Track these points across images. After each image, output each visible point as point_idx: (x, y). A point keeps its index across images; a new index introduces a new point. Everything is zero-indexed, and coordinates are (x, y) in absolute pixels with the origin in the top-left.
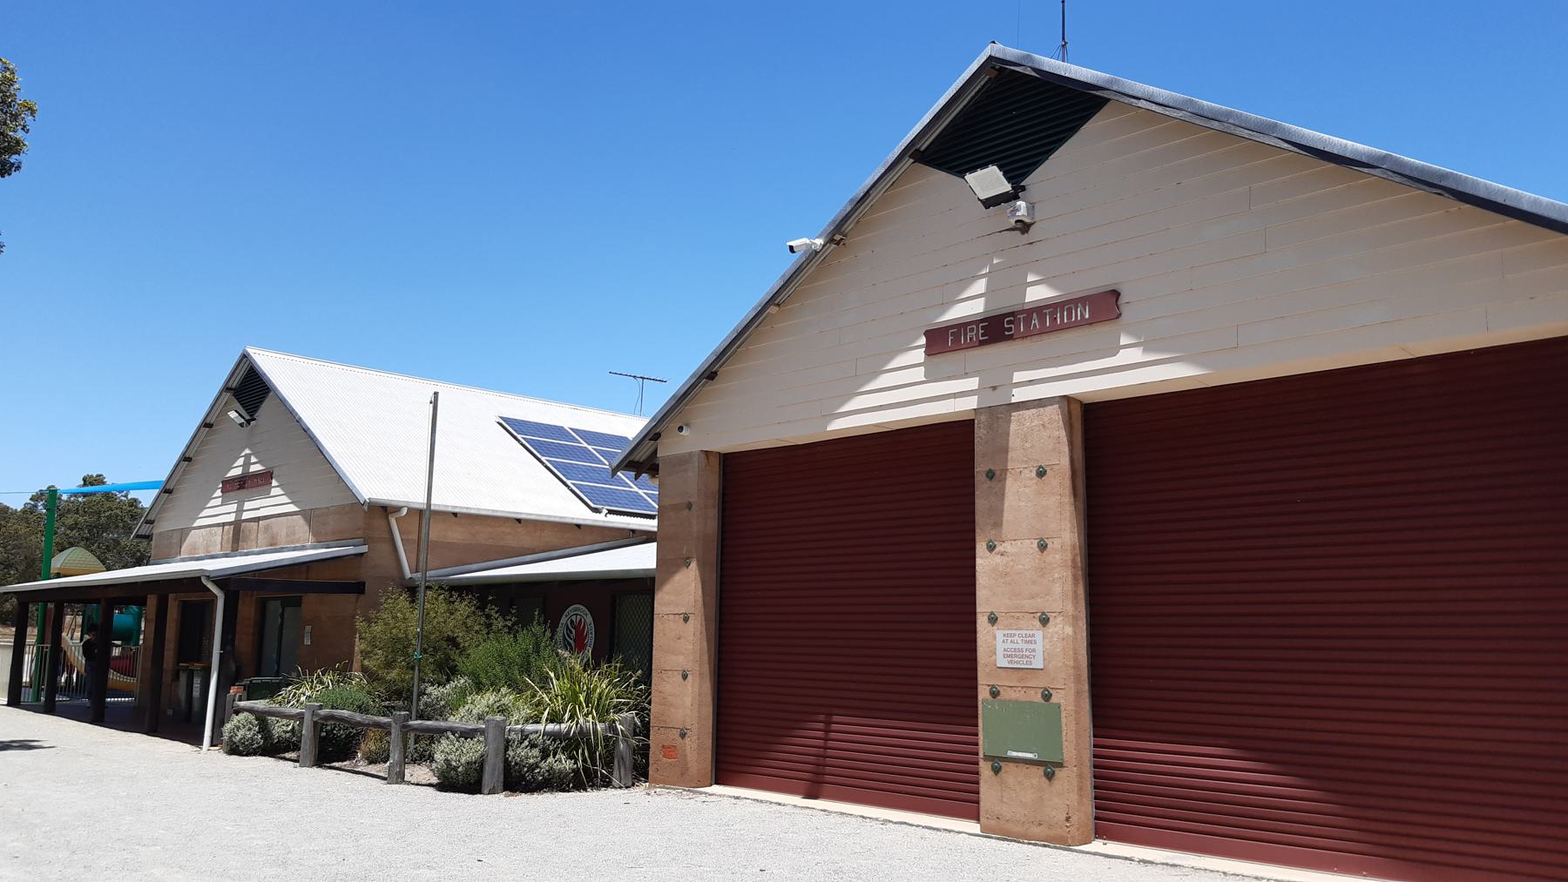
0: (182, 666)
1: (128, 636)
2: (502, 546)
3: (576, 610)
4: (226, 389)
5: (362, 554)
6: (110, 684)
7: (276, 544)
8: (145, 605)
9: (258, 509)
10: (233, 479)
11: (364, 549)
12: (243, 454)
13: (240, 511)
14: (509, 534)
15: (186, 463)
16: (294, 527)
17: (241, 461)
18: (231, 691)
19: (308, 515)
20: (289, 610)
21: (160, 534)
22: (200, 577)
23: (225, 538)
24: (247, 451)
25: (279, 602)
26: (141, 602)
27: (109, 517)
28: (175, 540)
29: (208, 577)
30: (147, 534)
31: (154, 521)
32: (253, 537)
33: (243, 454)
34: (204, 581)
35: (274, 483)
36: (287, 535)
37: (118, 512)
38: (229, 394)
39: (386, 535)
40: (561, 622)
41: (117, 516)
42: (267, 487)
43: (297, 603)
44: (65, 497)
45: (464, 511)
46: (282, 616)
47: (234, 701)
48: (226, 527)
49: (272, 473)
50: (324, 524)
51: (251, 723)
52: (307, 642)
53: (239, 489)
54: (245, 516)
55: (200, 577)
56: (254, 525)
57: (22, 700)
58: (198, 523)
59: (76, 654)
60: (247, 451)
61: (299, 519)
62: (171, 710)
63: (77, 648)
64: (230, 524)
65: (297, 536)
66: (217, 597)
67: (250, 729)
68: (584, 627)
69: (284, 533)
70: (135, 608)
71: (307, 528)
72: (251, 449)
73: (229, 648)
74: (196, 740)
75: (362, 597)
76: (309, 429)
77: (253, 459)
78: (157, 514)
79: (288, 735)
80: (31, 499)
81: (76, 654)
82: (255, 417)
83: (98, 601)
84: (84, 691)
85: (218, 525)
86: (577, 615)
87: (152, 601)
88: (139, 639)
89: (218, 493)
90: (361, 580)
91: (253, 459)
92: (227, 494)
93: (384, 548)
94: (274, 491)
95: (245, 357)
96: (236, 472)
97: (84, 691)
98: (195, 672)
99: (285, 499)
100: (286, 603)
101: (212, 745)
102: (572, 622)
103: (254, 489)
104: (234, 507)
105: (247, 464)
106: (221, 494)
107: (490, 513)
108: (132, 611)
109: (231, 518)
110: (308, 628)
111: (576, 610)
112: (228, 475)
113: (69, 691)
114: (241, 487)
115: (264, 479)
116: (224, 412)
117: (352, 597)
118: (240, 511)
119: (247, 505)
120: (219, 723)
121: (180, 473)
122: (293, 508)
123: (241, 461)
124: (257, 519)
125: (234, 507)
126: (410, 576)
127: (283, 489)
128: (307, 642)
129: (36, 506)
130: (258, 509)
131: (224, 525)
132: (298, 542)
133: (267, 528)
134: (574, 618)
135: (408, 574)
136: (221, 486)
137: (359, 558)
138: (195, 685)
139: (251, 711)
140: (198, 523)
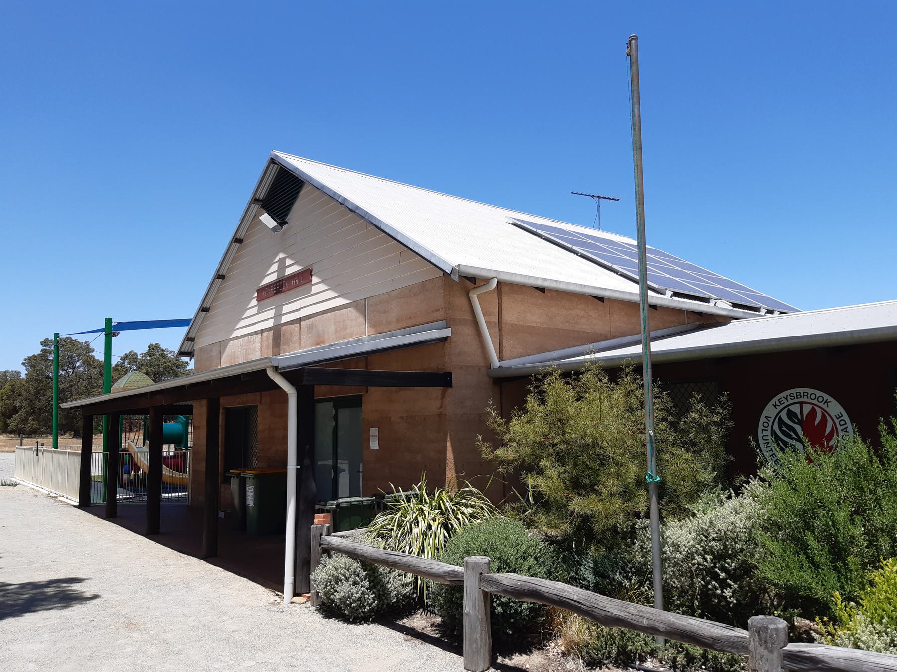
0: (233, 473)
1: (179, 440)
2: (578, 332)
3: (798, 395)
4: (255, 200)
5: (445, 339)
6: (164, 479)
7: (324, 343)
8: (191, 413)
9: (299, 310)
10: (268, 286)
11: (447, 332)
12: (277, 260)
13: (278, 315)
14: (582, 317)
15: (221, 280)
16: (344, 321)
17: (275, 267)
18: (316, 521)
19: (361, 306)
20: (345, 415)
21: (201, 349)
22: (264, 371)
23: (264, 344)
24: (281, 256)
25: (331, 404)
26: (188, 411)
27: (164, 368)
28: (215, 353)
29: (276, 369)
30: (189, 351)
31: (194, 338)
32: (295, 338)
33: (277, 260)
34: (271, 374)
35: (315, 279)
36: (336, 331)
37: (169, 364)
38: (257, 206)
39: (468, 316)
40: (765, 413)
41: (169, 366)
42: (308, 285)
43: (356, 402)
44: (139, 357)
45: (553, 285)
46: (336, 417)
47: (321, 535)
48: (265, 334)
49: (312, 271)
50: (385, 312)
51: (355, 574)
52: (374, 445)
53: (275, 294)
54: (285, 319)
55: (264, 371)
56: (296, 327)
57: (92, 502)
58: (236, 334)
59: (142, 459)
60: (281, 256)
61: (351, 312)
62: (220, 516)
63: (142, 454)
64: (269, 329)
65: (348, 331)
66: (287, 394)
67: (355, 583)
68: (824, 420)
69: (332, 328)
70: (182, 418)
71: (361, 319)
72: (284, 252)
73: (307, 462)
74: (274, 583)
75: (450, 390)
76: (358, 207)
77: (288, 262)
78: (196, 333)
79: (408, 589)
80: (121, 359)
81: (142, 459)
82: (286, 220)
83: (143, 412)
84: (144, 487)
85: (256, 333)
86: (801, 403)
87: (200, 409)
88: (187, 442)
89: (254, 302)
90: (448, 370)
91: (288, 262)
92: (262, 302)
93: (469, 330)
94: (315, 289)
95: (273, 161)
96: (270, 278)
97: (144, 487)
98: (248, 480)
99: (331, 294)
100: (340, 403)
101: (295, 594)
102: (791, 414)
103: (292, 291)
104: (271, 313)
105: (282, 266)
106: (256, 303)
107: (577, 289)
108: (181, 421)
109: (270, 323)
110: (374, 431)
111: (798, 395)
112: (261, 285)
113: (134, 486)
114: (278, 292)
115: (304, 277)
116: (256, 216)
117: (436, 391)
118: (278, 315)
119: (286, 309)
120: (304, 566)
121: (215, 291)
122: (341, 301)
123: (275, 267)
124: (299, 320)
125: (271, 313)
126: (499, 365)
127: (327, 284)
128: (374, 445)
129: (124, 363)
130: (299, 310)
131: (262, 331)
132: (351, 337)
133: (311, 327)
134: (796, 409)
135: (496, 363)
136: (256, 295)
137: (441, 344)
138: (248, 494)
139: (352, 554)
140: (236, 334)
